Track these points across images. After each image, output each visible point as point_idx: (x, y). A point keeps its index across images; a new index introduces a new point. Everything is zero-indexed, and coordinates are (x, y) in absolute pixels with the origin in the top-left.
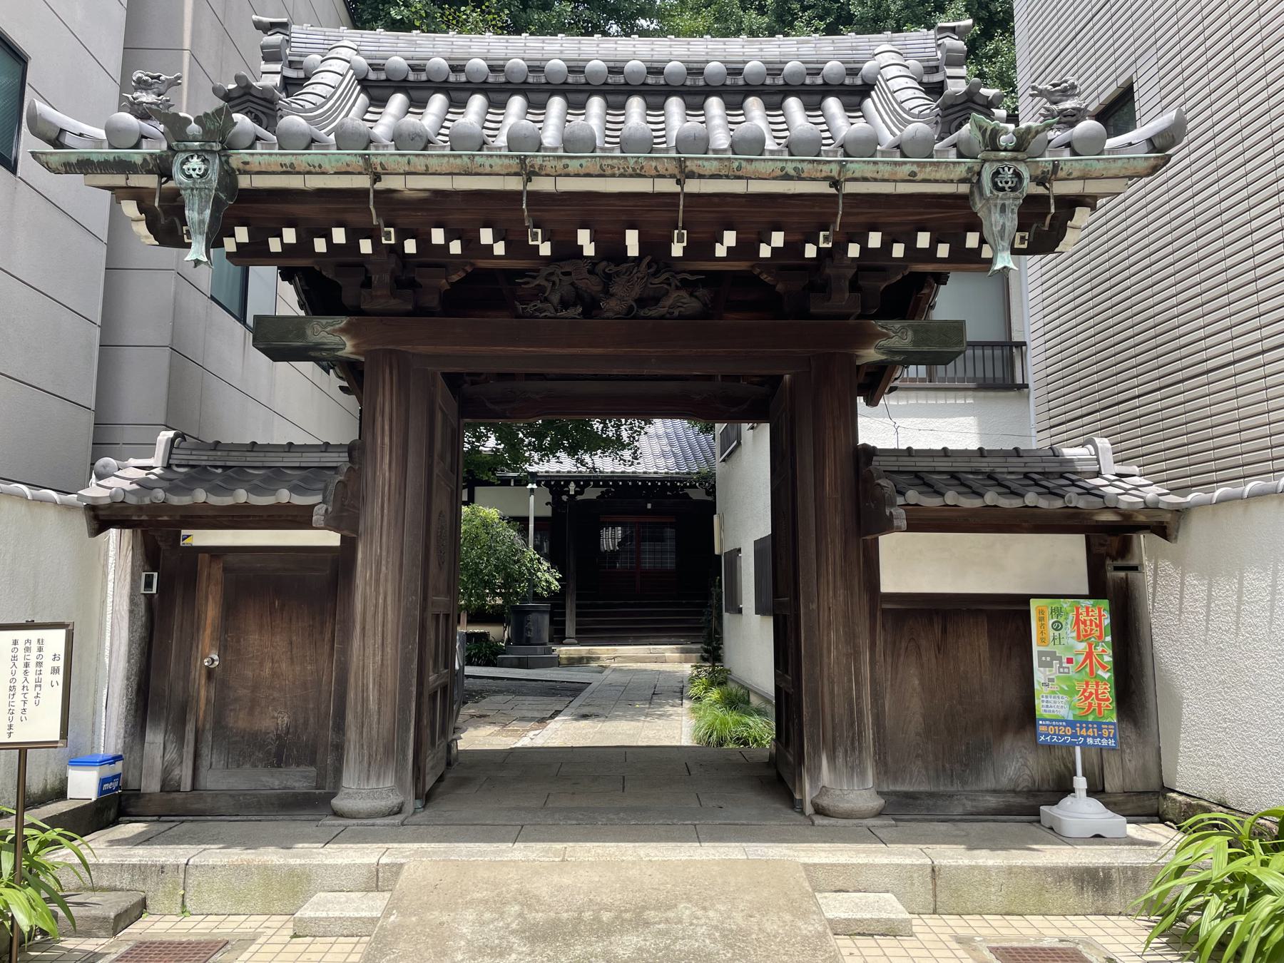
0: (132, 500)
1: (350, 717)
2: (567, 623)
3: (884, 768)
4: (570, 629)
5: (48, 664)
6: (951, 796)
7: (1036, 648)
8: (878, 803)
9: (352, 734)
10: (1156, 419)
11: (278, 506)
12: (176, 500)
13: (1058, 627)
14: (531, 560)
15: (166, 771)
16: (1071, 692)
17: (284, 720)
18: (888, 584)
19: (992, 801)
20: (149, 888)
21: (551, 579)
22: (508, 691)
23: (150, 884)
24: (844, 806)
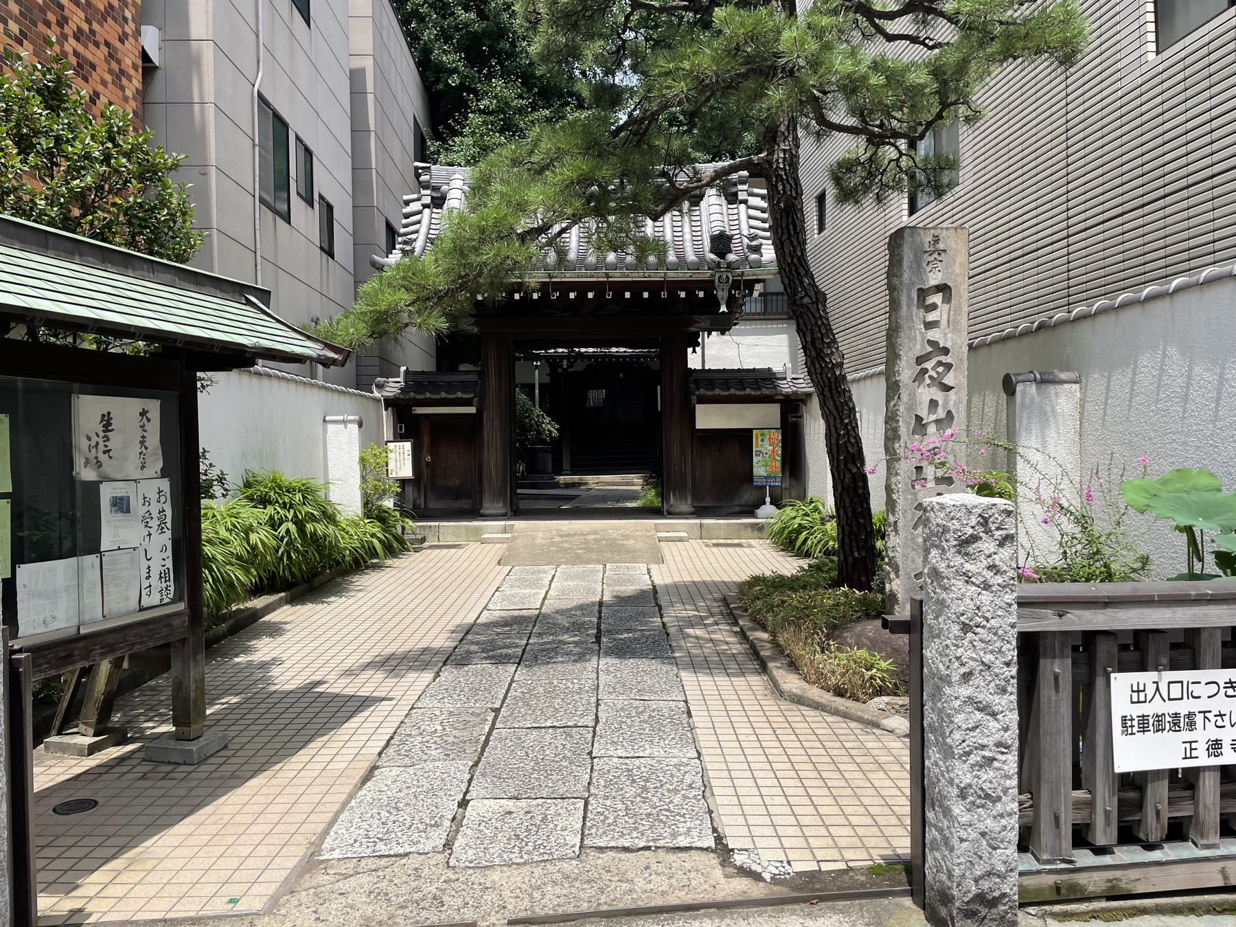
0: (402, 397)
1: (485, 480)
3: (695, 498)
4: (566, 465)
5: (406, 453)
6: (721, 507)
7: (754, 449)
8: (691, 509)
9: (486, 486)
11: (457, 398)
12: (418, 397)
13: (763, 441)
16: (766, 465)
17: (458, 482)
18: (699, 426)
19: (737, 509)
23: (427, 531)
24: (678, 510)
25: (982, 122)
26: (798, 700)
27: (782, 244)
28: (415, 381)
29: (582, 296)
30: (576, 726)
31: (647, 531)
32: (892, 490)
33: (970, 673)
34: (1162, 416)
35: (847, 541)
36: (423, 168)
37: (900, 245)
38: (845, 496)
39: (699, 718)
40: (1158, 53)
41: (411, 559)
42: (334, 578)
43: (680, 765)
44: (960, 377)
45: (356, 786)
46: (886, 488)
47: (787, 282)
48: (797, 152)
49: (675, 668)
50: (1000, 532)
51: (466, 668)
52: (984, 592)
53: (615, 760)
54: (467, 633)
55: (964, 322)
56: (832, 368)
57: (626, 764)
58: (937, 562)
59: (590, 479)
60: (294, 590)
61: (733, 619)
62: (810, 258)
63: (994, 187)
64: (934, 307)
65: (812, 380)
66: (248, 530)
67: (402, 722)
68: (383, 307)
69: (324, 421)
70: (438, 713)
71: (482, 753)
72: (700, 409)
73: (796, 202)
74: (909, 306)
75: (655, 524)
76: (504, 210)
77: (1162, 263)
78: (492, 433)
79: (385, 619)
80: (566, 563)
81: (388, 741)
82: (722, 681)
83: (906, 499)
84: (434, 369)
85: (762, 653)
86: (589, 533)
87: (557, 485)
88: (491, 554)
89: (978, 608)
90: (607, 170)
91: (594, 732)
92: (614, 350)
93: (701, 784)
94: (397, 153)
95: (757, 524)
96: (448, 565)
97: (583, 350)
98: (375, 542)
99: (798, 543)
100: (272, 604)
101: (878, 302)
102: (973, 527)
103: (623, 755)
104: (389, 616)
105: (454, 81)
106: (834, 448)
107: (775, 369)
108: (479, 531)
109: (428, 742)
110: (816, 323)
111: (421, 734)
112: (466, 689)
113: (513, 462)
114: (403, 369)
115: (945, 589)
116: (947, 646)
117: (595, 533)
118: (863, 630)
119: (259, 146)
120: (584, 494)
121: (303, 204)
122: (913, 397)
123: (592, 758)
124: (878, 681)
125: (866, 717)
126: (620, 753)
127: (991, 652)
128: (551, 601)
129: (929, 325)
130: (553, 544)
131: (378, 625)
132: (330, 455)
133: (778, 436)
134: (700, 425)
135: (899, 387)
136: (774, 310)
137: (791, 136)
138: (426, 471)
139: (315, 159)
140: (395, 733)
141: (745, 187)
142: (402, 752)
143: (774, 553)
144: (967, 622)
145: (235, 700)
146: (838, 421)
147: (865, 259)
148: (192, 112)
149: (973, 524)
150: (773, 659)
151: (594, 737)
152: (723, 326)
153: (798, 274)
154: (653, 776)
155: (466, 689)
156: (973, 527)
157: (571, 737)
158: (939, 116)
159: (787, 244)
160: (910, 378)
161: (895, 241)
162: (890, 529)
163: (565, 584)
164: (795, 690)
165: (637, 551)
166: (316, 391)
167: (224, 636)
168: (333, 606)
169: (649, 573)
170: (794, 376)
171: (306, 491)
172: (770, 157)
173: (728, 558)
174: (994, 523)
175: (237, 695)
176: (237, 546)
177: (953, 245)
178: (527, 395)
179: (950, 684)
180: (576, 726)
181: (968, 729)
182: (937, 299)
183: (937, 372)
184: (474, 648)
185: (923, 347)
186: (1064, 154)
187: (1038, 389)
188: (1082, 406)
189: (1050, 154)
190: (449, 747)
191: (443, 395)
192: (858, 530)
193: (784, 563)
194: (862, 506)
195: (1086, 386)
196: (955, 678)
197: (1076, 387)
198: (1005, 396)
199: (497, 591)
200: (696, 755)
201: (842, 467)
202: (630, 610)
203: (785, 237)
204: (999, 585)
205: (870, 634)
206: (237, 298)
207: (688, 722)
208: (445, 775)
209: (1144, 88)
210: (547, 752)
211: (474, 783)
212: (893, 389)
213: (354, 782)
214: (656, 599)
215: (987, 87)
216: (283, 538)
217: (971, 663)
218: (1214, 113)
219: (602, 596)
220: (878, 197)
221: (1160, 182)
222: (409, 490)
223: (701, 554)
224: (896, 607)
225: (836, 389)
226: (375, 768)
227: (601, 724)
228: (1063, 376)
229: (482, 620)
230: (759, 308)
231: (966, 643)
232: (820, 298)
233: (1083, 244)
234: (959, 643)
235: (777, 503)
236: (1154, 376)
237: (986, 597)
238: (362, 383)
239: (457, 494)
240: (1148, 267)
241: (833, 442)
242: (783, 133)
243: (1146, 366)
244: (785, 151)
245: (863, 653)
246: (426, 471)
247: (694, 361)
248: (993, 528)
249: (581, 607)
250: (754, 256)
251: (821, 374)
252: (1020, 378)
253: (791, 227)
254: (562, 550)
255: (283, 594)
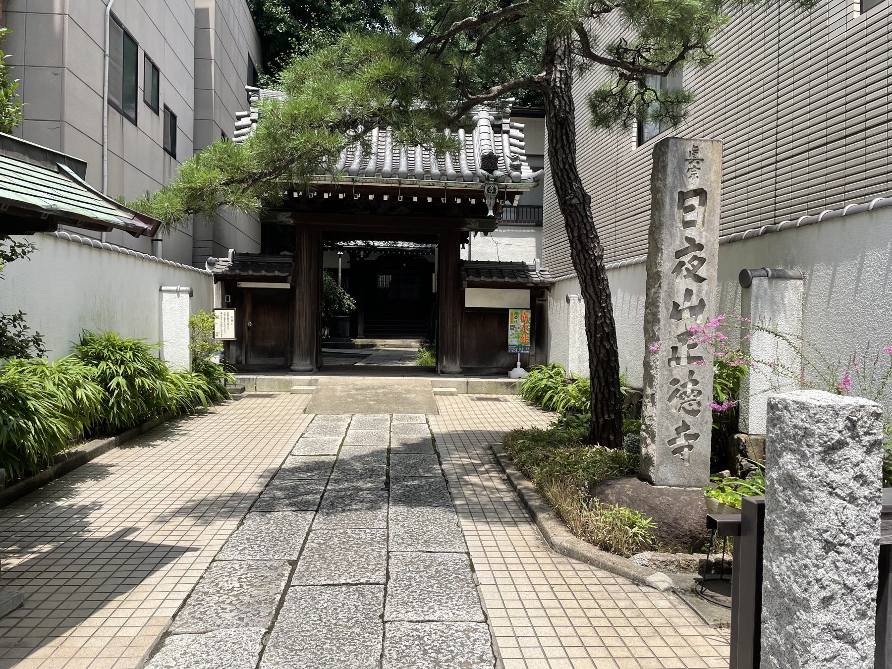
0: (229, 273)
1: (296, 343)
2: (359, 327)
3: (463, 361)
4: (361, 330)
5: (230, 319)
6: (482, 369)
8: (459, 370)
9: (296, 347)
10: (822, 196)
12: (243, 273)
13: (516, 318)
14: (340, 293)
15: (237, 358)
16: (518, 337)
17: (273, 343)
18: (467, 305)
19: (495, 370)
20: (245, 384)
21: (351, 304)
22: (331, 356)
24: (449, 370)
25: (713, 64)
26: (568, 553)
27: (556, 152)
28: (241, 261)
29: (378, 198)
30: (368, 583)
31: (425, 386)
32: (651, 367)
33: (832, 598)
34: (888, 310)
35: (599, 405)
36: (252, 91)
37: (665, 153)
38: (599, 368)
39: (482, 573)
40: (862, 12)
41: (231, 406)
42: (162, 423)
43: (469, 631)
44: (712, 270)
45: (143, 659)
46: (644, 364)
47: (559, 185)
48: (571, 74)
49: (456, 517)
50: (867, 438)
51: (269, 516)
52: (849, 505)
53: (407, 624)
54: (272, 478)
55: (717, 221)
56: (594, 260)
57: (417, 630)
58: (794, 468)
59: (379, 342)
60: (123, 434)
61: (499, 464)
62: (578, 162)
63: (712, 123)
64: (692, 208)
65: (576, 269)
66: (75, 386)
67: (202, 577)
68: (198, 184)
69: (160, 290)
70: (237, 567)
71: (276, 617)
72: (468, 291)
73: (570, 117)
74: (672, 206)
75: (432, 381)
76: (315, 102)
77: (862, 183)
78: (303, 306)
79: (201, 463)
80: (360, 413)
81: (185, 600)
82: (498, 529)
83: (663, 375)
84: (258, 251)
85: (531, 503)
86: (379, 388)
87: (353, 346)
88: (298, 403)
89: (843, 524)
90: (411, 70)
91: (385, 589)
92: (400, 244)
93: (491, 655)
94: (233, 80)
95: (511, 383)
96: (262, 412)
97: (376, 243)
98: (200, 392)
99: (545, 400)
100: (101, 447)
101: (610, 213)
102: (840, 432)
103: (413, 618)
104: (205, 460)
105: (281, 28)
106: (593, 328)
107: (527, 263)
108: (289, 384)
109: (223, 602)
110: (583, 220)
111: (218, 592)
112: (267, 539)
113: (319, 329)
114: (231, 251)
115: (806, 501)
116: (806, 566)
117: (384, 387)
118: (622, 488)
119: (110, 57)
120: (374, 353)
121: (149, 111)
122: (671, 285)
123: (384, 622)
124: (640, 538)
125: (632, 573)
126: (412, 616)
127: (855, 574)
128: (347, 448)
129: (687, 224)
130: (349, 396)
131: (195, 468)
132: (165, 319)
133: (528, 314)
134: (468, 304)
135: (660, 276)
136: (524, 219)
137: (566, 60)
138: (247, 334)
139: (160, 74)
140: (193, 590)
141: (508, 121)
142: (197, 615)
143: (524, 407)
144: (831, 539)
145: (47, 548)
146: (597, 305)
147: (600, 180)
148: (51, 22)
149: (841, 428)
150: (542, 509)
151: (385, 596)
152: (488, 228)
153: (569, 178)
154: (444, 646)
155: (267, 539)
156: (840, 432)
157: (364, 597)
158: (682, 57)
159: (560, 151)
160: (670, 269)
161: (660, 149)
162: (647, 400)
163: (360, 431)
164: (565, 544)
165: (417, 403)
166: (153, 265)
167: (51, 479)
168: (158, 448)
169: (427, 422)
170: (541, 269)
171: (137, 350)
172: (548, 77)
173: (490, 411)
174: (862, 427)
175: (48, 543)
176: (63, 399)
177: (710, 155)
178: (332, 277)
179: (807, 609)
180: (368, 583)
181: (825, 659)
182: (694, 201)
183: (693, 265)
184: (279, 494)
185: (681, 242)
186: (775, 96)
187: (770, 283)
188: (805, 300)
189: (762, 96)
190: (243, 608)
191: (263, 273)
192: (609, 396)
193: (534, 416)
194: (613, 377)
195: (810, 280)
196: (814, 603)
197: (800, 283)
198: (740, 288)
199: (301, 437)
200: (483, 618)
201: (598, 344)
202: (414, 459)
203: (559, 146)
204: (865, 497)
205: (629, 493)
206: (48, 165)
207: (472, 578)
208: (236, 646)
209: (849, 41)
210: (340, 616)
211: (265, 655)
212: (654, 279)
213: (142, 655)
214: (435, 446)
215: (722, 33)
216: (113, 391)
217: (833, 586)
218: (869, 80)
219: (390, 443)
220: (625, 123)
221: (806, 139)
222: (233, 348)
223: (468, 407)
224: (651, 468)
225: (597, 278)
226: (167, 634)
227: (391, 580)
228: (790, 273)
229: (287, 465)
230: (513, 216)
231: (827, 563)
232: (586, 200)
233: (789, 168)
234: (820, 563)
235: (526, 367)
236: (880, 275)
237: (851, 511)
238: (197, 260)
239: (273, 353)
240: (848, 187)
241: (592, 322)
242: (560, 57)
243: (873, 266)
244: (561, 72)
245: (625, 512)
246: (247, 334)
247: (464, 255)
248: (861, 433)
249: (372, 454)
250: (515, 173)
251: (585, 265)
252: (756, 273)
253: (564, 137)
254: (357, 401)
255: (113, 438)
